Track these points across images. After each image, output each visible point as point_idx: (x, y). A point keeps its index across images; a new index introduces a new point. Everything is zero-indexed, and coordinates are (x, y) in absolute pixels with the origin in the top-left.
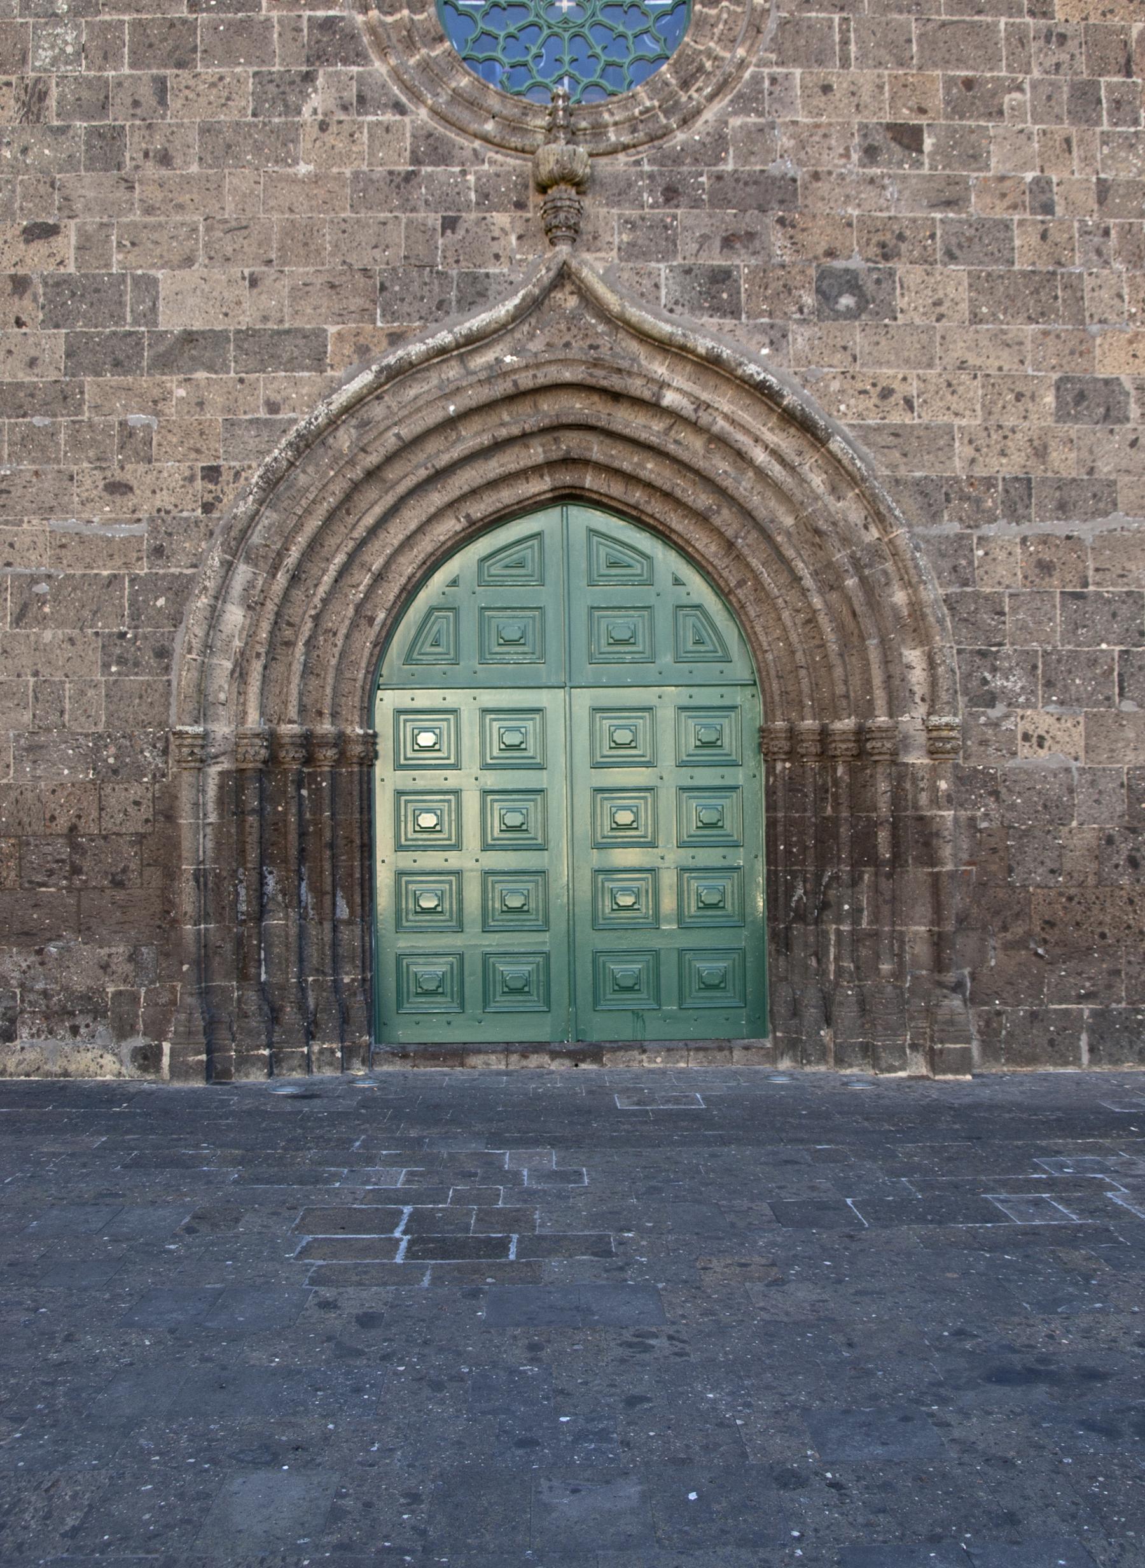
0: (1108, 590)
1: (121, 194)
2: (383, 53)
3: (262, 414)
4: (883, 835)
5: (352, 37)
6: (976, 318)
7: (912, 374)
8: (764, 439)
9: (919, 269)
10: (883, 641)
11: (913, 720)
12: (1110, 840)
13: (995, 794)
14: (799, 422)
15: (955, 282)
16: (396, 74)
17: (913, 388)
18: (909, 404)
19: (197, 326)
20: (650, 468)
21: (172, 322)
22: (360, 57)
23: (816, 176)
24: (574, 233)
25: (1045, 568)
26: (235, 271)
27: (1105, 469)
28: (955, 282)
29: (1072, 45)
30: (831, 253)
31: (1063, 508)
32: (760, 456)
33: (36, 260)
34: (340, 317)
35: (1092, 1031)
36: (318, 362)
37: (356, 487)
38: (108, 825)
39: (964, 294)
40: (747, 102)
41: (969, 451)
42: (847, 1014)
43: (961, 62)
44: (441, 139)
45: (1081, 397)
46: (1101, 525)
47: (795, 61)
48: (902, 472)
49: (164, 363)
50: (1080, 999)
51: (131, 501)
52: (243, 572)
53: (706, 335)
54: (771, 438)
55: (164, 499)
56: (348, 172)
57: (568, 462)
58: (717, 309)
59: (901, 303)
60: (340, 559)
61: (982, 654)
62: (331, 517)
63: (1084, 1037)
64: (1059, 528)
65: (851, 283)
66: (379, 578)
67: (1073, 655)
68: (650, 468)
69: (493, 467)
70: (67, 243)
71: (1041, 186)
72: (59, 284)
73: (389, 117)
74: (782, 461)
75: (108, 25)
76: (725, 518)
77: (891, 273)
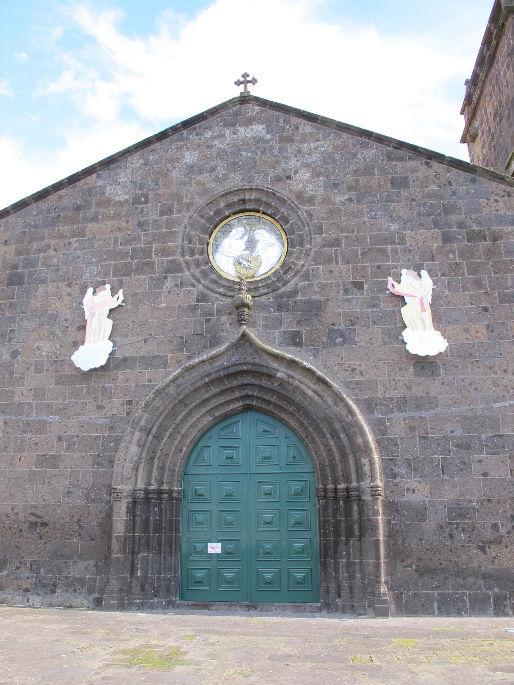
0: (436, 435)
2: (189, 269)
3: (147, 383)
6: (384, 343)
12: (442, 528)
16: (193, 275)
17: (363, 368)
18: (362, 373)
22: (182, 271)
27: (432, 393)
30: (333, 325)
31: (418, 407)
35: (438, 601)
36: (165, 366)
41: (383, 389)
42: (345, 593)
47: (320, 264)
48: (360, 397)
50: (433, 589)
51: (104, 411)
54: (314, 387)
55: (114, 411)
56: (176, 306)
59: (358, 339)
61: (391, 460)
64: (417, 414)
65: (341, 334)
73: (190, 288)
74: (318, 395)
77: (354, 330)
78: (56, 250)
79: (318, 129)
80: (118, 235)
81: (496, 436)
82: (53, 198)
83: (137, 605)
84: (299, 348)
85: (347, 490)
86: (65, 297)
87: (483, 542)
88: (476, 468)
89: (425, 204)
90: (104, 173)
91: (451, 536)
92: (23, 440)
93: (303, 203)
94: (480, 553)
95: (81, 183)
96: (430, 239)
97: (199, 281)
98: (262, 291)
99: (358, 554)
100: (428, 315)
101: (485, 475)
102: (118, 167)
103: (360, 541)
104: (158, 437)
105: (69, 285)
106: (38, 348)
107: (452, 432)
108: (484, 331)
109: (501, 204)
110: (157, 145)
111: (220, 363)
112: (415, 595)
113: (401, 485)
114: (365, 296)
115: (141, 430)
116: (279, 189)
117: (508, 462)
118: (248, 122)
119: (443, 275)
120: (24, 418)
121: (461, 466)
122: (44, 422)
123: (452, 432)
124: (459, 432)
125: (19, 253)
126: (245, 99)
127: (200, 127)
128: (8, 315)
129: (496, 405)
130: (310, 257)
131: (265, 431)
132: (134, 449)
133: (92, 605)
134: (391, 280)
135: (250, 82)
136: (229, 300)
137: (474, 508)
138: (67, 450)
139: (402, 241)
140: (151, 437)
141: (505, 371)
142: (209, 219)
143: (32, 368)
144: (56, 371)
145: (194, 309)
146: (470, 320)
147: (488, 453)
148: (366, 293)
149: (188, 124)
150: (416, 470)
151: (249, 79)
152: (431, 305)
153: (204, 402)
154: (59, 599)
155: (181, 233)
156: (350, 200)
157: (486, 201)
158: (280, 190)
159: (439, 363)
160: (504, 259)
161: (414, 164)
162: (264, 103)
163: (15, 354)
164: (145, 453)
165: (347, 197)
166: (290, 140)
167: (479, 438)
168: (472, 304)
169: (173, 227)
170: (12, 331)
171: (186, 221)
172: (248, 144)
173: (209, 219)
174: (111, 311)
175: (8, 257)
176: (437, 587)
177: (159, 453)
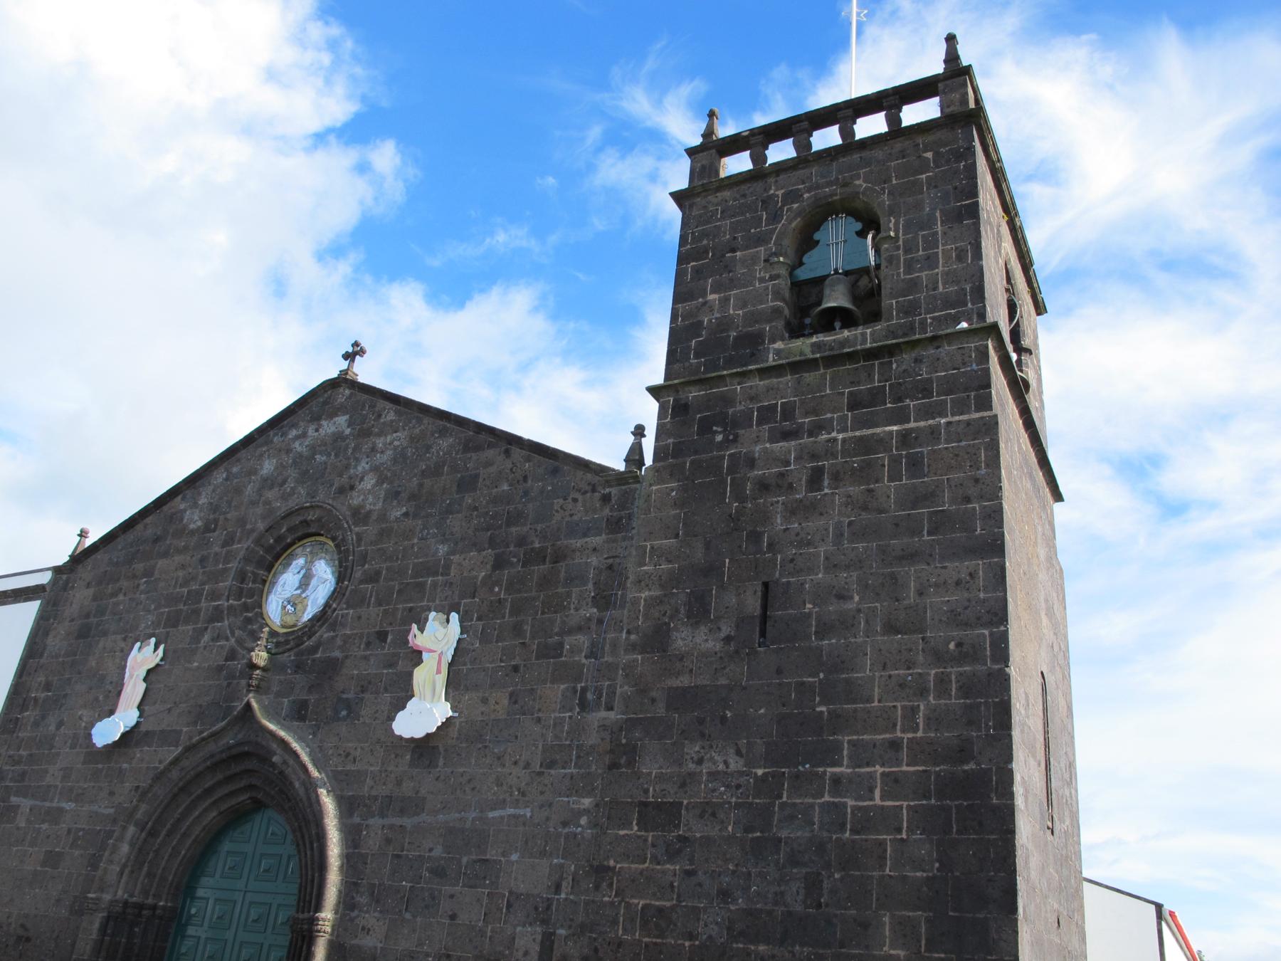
27: (423, 792)
31: (402, 812)
46: (416, 819)
64: (397, 821)
80: (181, 573)
81: (480, 860)
89: (487, 513)
90: (189, 493)
95: (165, 508)
96: (475, 565)
100: (441, 679)
101: (453, 917)
104: (153, 834)
105: (124, 639)
111: (225, 741)
113: (357, 921)
114: (386, 651)
115: (136, 825)
123: (431, 850)
124: (438, 851)
129: (491, 815)
134: (414, 626)
142: (269, 549)
145: (220, 669)
146: (492, 686)
147: (464, 886)
150: (378, 901)
152: (450, 665)
153: (208, 792)
156: (406, 514)
159: (441, 749)
160: (560, 590)
161: (490, 453)
168: (501, 661)
171: (242, 554)
173: (269, 549)
174: (149, 671)
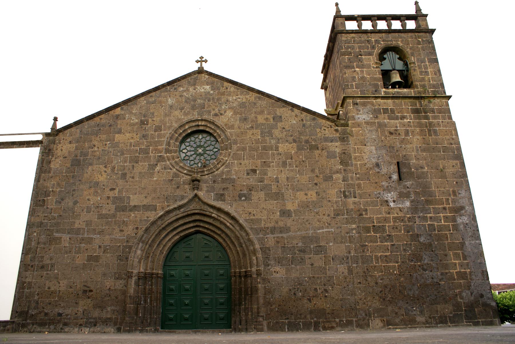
0: (289, 246)
1: (126, 183)
2: (169, 160)
3: (146, 219)
4: (249, 289)
5: (164, 158)
6: (266, 200)
7: (254, 210)
8: (228, 222)
9: (256, 192)
10: (249, 255)
11: (254, 269)
12: (290, 290)
13: (269, 282)
14: (233, 218)
15: (262, 195)
16: (171, 164)
17: (255, 212)
18: (254, 215)
19: (136, 204)
20: (211, 227)
21: (132, 204)
22: (166, 161)
23: (239, 178)
24: (198, 189)
25: (278, 242)
26: (143, 196)
27: (288, 225)
28: (262, 195)
29: (282, 155)
30: (241, 190)
31: (281, 232)
32: (228, 224)
33: (111, 194)
34: (159, 203)
35: (288, 325)
36: (156, 210)
37: (161, 231)
38: (116, 288)
39: (264, 196)
40: (227, 167)
41: (264, 223)
42: (243, 322)
43: (263, 159)
44: (178, 174)
45: (284, 213)
46: (288, 234)
47: (236, 160)
48: (253, 226)
49: (131, 210)
50: (285, 319)
51: (124, 233)
52: (141, 244)
53: (218, 204)
54: (230, 221)
55: (129, 233)
56: (162, 179)
57: (197, 226)
58: (222, 200)
59: (253, 198)
60: (158, 243)
61: (267, 257)
62: (156, 235)
63: (286, 326)
64: (281, 235)
65: (244, 195)
66: (165, 246)
67: (283, 257)
68: (211, 227)
69: (185, 227)
70: (116, 191)
71: (277, 178)
72: (114, 198)
73: (169, 170)
74: (232, 226)
75: (126, 157)
76: (223, 235)
77: (251, 193)
78: (98, 148)
79: (238, 89)
80: (132, 141)
82: (97, 119)
83: (140, 330)
84: (223, 202)
85: (246, 272)
86: (103, 173)
87: (310, 296)
88: (308, 261)
90: (125, 107)
91: (295, 294)
92: (79, 247)
93: (229, 128)
94: (308, 302)
95: (111, 112)
97: (174, 167)
98: (206, 173)
99: (250, 303)
101: (312, 265)
102: (132, 104)
103: (251, 297)
106: (89, 200)
107: (297, 244)
108: (315, 195)
109: (327, 131)
110: (153, 94)
112: (277, 322)
116: (217, 120)
117: (323, 258)
118: (202, 84)
119: (296, 167)
120: (81, 236)
121: (300, 260)
122: (92, 238)
123: (297, 244)
124: (300, 244)
125: (77, 148)
126: (201, 71)
127: (176, 85)
128: (71, 181)
129: (318, 231)
130: (231, 156)
131: (206, 244)
132: (139, 252)
133: (116, 331)
135: (203, 61)
136: (189, 177)
137: (306, 281)
138: (104, 252)
139: (277, 148)
140: (147, 246)
141: (324, 215)
143: (85, 210)
144: (98, 212)
146: (308, 190)
147: (314, 254)
148: (258, 176)
149: (170, 83)
151: (203, 59)
154: (98, 329)
155: (165, 142)
157: (319, 130)
158: (217, 121)
162: (210, 74)
163: (76, 203)
164: (144, 254)
165: (250, 125)
166: (223, 94)
167: (310, 247)
169: (161, 138)
170: (74, 190)
172: (201, 96)
175: (72, 150)
176: (288, 319)
177: (152, 254)
